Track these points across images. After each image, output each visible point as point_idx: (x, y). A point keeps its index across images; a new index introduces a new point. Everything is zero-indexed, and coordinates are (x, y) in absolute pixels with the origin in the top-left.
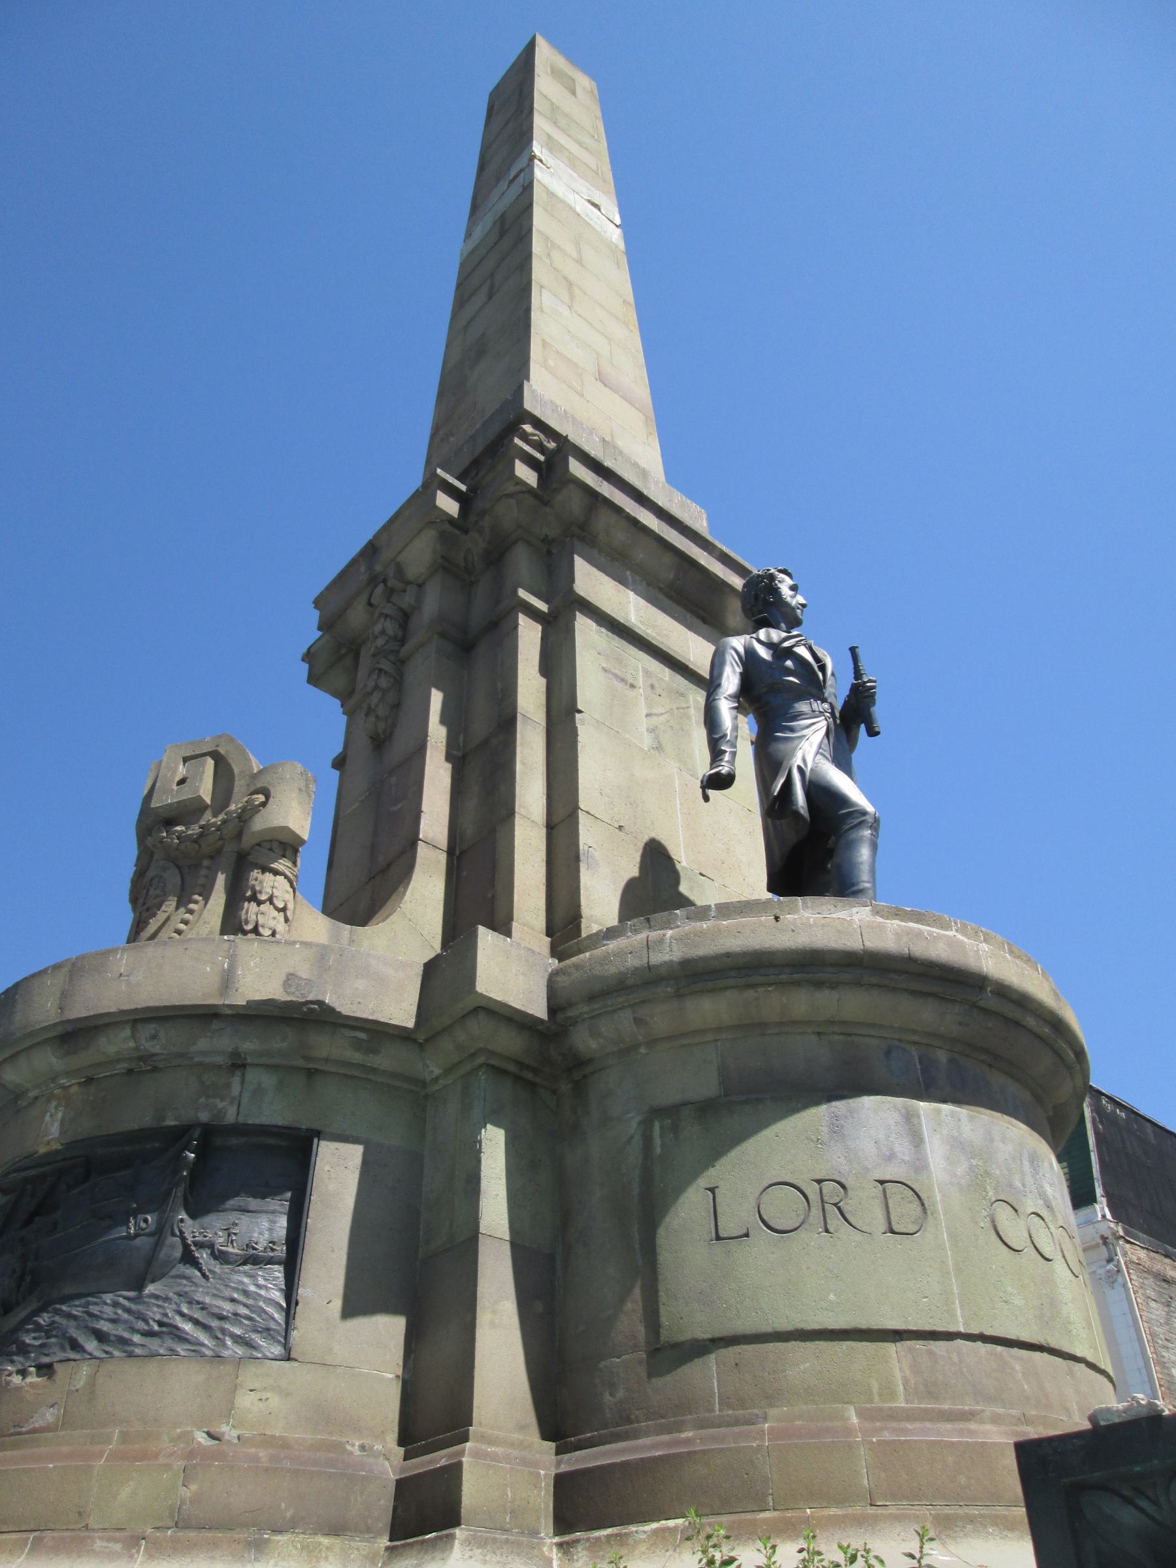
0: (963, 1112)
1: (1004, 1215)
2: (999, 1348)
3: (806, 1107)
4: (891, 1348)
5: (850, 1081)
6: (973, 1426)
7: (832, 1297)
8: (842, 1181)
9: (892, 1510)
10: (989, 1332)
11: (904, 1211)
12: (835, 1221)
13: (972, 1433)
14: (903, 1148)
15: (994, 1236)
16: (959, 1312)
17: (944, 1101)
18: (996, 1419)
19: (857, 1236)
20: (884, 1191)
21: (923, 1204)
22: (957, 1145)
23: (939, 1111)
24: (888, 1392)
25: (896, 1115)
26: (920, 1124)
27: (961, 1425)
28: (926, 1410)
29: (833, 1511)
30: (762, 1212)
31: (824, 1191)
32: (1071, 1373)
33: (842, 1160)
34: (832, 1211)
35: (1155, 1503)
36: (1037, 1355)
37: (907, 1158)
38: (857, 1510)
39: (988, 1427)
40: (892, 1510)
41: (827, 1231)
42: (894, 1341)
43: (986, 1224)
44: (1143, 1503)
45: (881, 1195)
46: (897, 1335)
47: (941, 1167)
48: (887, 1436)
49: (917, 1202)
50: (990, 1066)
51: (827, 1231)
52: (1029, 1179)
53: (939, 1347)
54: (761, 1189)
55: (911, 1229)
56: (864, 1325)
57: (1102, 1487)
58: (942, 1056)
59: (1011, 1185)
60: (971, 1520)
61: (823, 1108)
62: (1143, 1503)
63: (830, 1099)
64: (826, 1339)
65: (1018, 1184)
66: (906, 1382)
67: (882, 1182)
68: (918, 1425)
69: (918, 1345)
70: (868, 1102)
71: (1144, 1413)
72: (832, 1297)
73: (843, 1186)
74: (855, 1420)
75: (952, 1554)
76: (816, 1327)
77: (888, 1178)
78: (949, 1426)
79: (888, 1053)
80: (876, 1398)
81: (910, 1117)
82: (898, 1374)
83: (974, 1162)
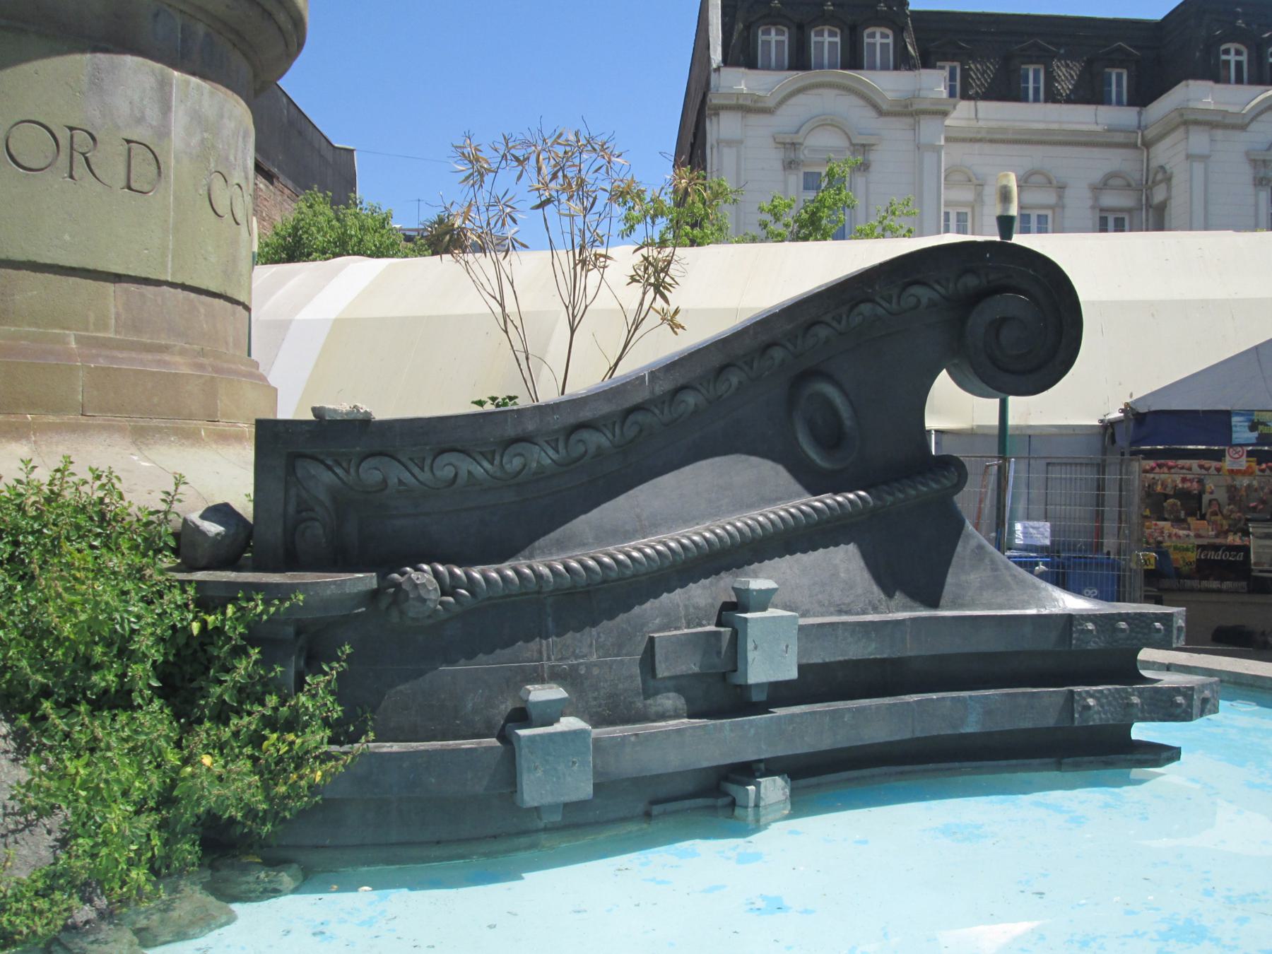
0: (206, 86)
1: (218, 183)
2: (193, 295)
3: (71, 51)
4: (110, 287)
5: (117, 38)
6: (167, 357)
7: (67, 237)
8: (94, 133)
9: (99, 421)
10: (188, 282)
11: (144, 168)
12: (80, 169)
13: (166, 364)
14: (152, 114)
15: (207, 203)
16: (170, 265)
17: (194, 74)
18: (183, 352)
19: (98, 187)
20: (129, 150)
21: (159, 168)
22: (197, 117)
23: (188, 83)
24: (102, 324)
25: (152, 80)
26: (171, 92)
27: (158, 357)
28: (133, 343)
29: (51, 418)
30: (11, 146)
31: (75, 140)
32: (234, 313)
33: (97, 113)
34: (79, 160)
35: (347, 471)
36: (216, 301)
37: (154, 123)
38: (70, 418)
39: (178, 359)
40: (99, 421)
41: (71, 177)
42: (114, 282)
43: (203, 191)
44: (338, 470)
45: (126, 153)
46: (117, 278)
47: (180, 137)
48: (102, 363)
49: (155, 166)
50: (234, 45)
51: (71, 177)
52: (240, 155)
53: (149, 290)
54: (12, 123)
55: (146, 188)
56: (91, 267)
57: (313, 458)
58: (201, 29)
59: (227, 159)
60: (158, 430)
61: (88, 56)
62: (338, 470)
63: (95, 50)
64: (55, 273)
65: (232, 158)
66: (118, 316)
67: (128, 142)
68: (125, 355)
69: (133, 287)
70: (130, 60)
71: (361, 417)
72: (67, 237)
73: (93, 138)
74: (73, 345)
75: (149, 460)
76: (48, 261)
77: (135, 138)
78: (149, 357)
79: (156, 15)
80: (92, 327)
81: (164, 86)
82: (113, 310)
83: (206, 135)
